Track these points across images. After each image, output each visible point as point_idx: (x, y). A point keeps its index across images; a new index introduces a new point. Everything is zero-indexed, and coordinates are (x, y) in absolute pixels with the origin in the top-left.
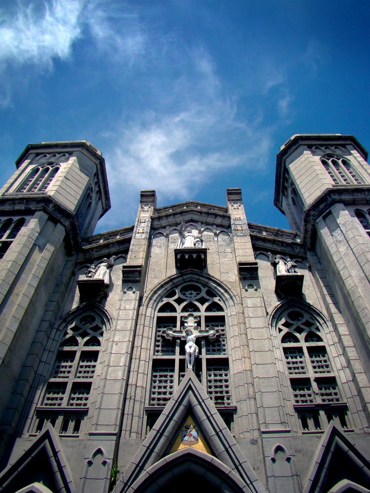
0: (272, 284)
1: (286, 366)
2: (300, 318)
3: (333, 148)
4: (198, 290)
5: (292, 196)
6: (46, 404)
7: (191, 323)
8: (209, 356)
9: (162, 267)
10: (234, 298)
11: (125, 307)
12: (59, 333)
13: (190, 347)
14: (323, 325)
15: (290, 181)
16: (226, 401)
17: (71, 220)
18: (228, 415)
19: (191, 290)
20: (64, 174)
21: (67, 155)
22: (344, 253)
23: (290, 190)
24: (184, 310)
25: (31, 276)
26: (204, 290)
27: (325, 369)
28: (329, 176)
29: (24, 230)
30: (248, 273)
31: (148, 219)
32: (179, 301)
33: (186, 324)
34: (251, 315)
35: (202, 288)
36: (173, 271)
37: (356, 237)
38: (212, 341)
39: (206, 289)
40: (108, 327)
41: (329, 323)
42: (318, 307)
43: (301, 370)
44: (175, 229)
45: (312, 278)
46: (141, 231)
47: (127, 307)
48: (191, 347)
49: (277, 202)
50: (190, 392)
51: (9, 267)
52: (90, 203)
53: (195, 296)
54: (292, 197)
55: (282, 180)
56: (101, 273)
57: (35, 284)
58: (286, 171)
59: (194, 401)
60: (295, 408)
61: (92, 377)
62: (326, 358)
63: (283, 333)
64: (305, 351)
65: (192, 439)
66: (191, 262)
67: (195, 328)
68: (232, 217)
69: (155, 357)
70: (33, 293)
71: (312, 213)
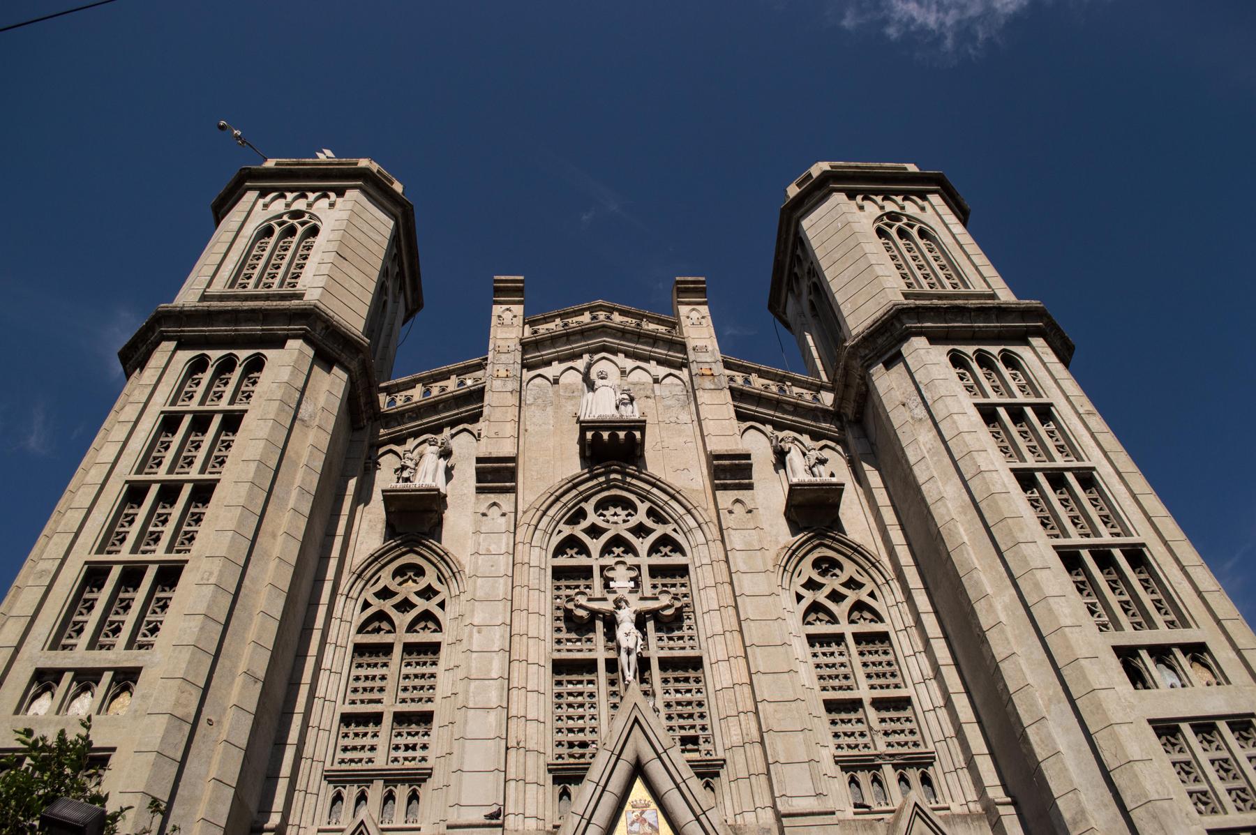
0: (779, 499)
1: (814, 673)
2: (837, 571)
3: (899, 199)
4: (629, 506)
5: (812, 297)
6: (343, 761)
7: (622, 581)
8: (666, 653)
9: (552, 461)
10: (704, 527)
11: (488, 550)
12: (351, 604)
13: (627, 635)
14: (883, 589)
15: (806, 266)
16: (703, 747)
17: (361, 356)
18: (708, 772)
19: (615, 507)
20: (334, 246)
21: (333, 195)
22: (929, 446)
23: (805, 285)
24: (606, 550)
25: (294, 493)
26: (643, 507)
27: (891, 681)
28: (891, 264)
29: (266, 378)
30: (731, 472)
31: (514, 345)
32: (594, 531)
33: (612, 584)
34: (743, 568)
35: (637, 502)
36: (573, 466)
37: (955, 417)
38: (666, 620)
39: (647, 505)
40: (455, 591)
41: (895, 585)
42: (872, 549)
43: (844, 683)
44: (571, 368)
45: (860, 490)
46: (503, 373)
47: (493, 549)
48: (627, 633)
49: (775, 306)
50: (639, 785)
51: (251, 475)
52: (385, 302)
53: (624, 521)
54: (811, 303)
55: (788, 260)
56: (429, 474)
57: (306, 508)
58: (800, 241)
59: (647, 754)
60: (837, 762)
61: (430, 700)
62: (891, 657)
63: (805, 604)
64: (850, 640)
65: (648, 830)
66: (612, 451)
67: (633, 591)
68: (690, 344)
69: (557, 656)
70: (303, 528)
71: (863, 352)
